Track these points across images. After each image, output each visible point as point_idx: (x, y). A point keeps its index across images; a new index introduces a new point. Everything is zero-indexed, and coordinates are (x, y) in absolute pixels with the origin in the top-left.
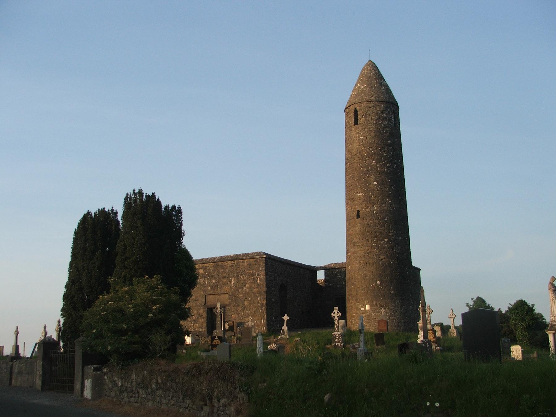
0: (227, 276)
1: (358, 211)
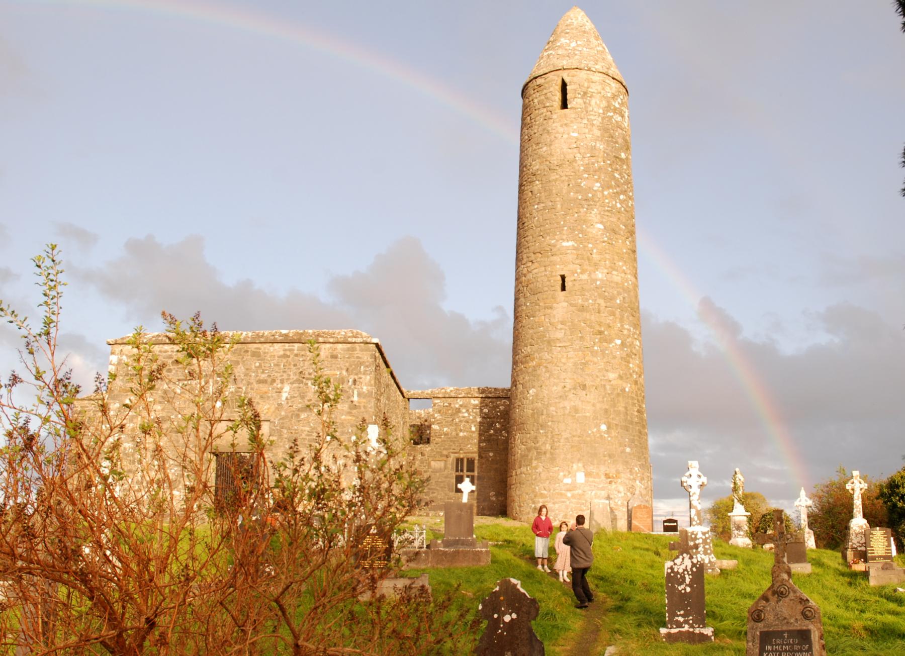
0: (269, 380)
1: (563, 278)
